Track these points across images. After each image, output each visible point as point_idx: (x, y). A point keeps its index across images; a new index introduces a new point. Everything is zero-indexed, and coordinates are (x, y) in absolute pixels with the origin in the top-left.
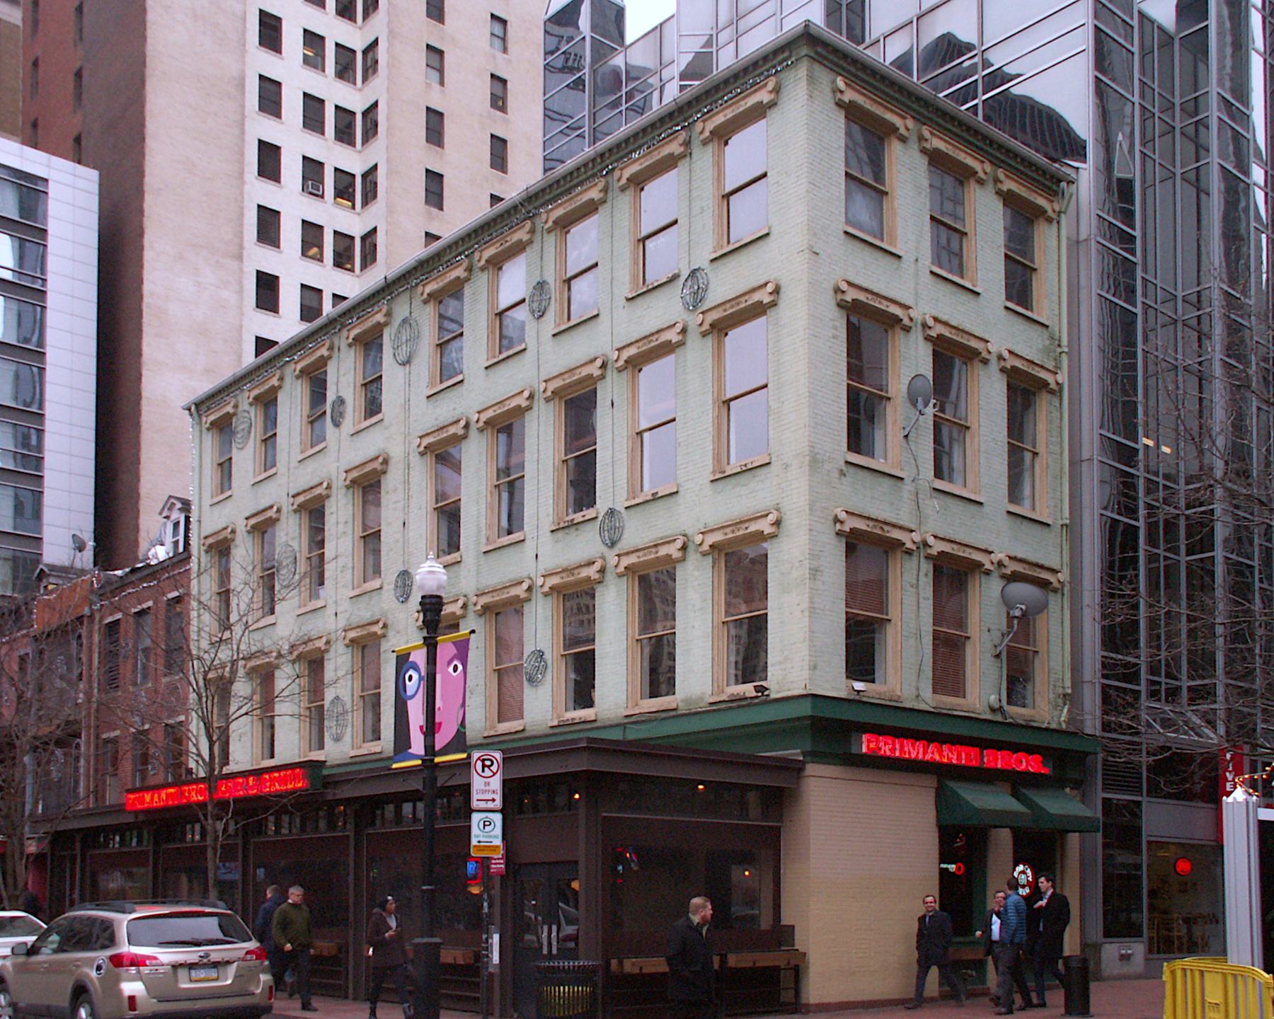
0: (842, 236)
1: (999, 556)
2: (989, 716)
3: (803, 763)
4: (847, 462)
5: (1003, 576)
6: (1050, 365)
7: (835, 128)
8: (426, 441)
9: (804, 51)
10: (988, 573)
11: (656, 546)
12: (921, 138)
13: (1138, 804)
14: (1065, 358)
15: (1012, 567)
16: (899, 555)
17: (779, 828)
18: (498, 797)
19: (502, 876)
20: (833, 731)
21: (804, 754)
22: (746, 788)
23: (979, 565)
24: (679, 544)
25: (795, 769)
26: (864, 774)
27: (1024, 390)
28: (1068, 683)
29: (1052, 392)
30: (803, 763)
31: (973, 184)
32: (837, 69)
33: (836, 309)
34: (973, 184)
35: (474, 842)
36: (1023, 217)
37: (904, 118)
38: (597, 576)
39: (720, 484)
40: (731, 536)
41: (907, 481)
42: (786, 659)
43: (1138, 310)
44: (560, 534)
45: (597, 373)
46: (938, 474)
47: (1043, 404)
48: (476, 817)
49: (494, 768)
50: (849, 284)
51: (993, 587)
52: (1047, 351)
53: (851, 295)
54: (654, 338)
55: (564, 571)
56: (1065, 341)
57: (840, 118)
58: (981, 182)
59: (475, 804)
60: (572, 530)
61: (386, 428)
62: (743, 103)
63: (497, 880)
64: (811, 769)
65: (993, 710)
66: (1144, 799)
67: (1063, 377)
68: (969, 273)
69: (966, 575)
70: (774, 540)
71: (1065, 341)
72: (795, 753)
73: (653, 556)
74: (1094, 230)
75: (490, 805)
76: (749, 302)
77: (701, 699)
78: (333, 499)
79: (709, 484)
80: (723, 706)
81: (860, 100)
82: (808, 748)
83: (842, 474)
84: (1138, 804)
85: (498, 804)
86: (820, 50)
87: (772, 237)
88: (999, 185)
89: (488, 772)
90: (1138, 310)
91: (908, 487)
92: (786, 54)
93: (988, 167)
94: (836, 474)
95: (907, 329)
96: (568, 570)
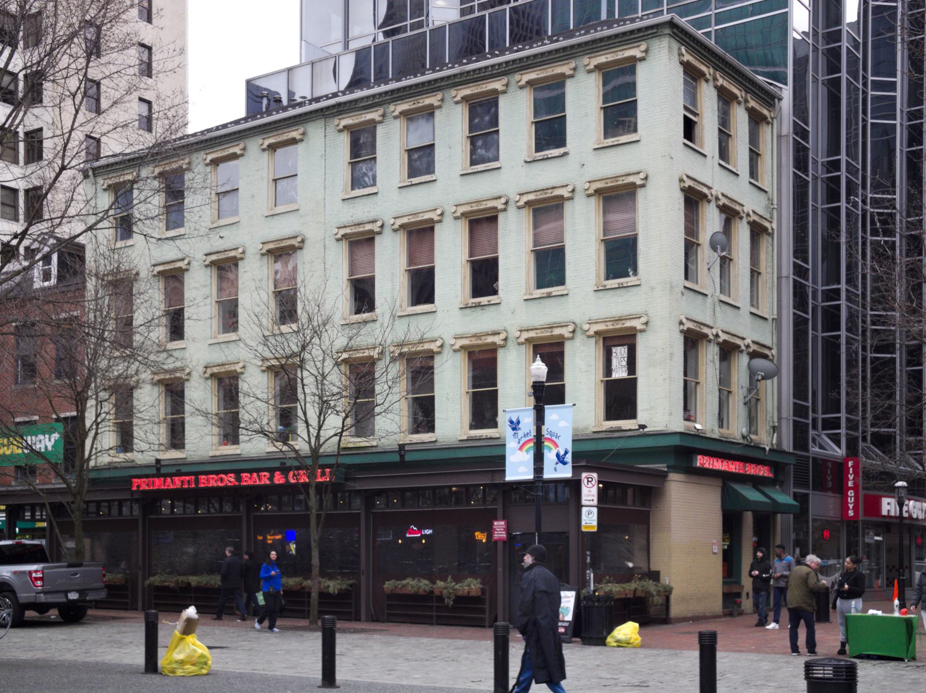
0: (682, 146)
1: (748, 341)
2: (741, 441)
3: (667, 472)
4: (685, 287)
5: (749, 354)
6: (768, 216)
7: (678, 76)
8: (342, 232)
9: (667, 31)
10: (710, 341)
11: (551, 328)
12: (681, 54)
13: (807, 495)
14: (775, 212)
15: (754, 347)
16: (705, 342)
17: (648, 512)
18: (596, 499)
19: (504, 542)
20: (683, 453)
21: (668, 467)
22: (625, 487)
23: (738, 347)
24: (571, 328)
25: (663, 476)
26: (694, 478)
27: (758, 231)
28: (776, 420)
29: (769, 234)
30: (667, 472)
31: (735, 104)
32: (682, 42)
33: (679, 191)
34: (735, 104)
35: (583, 523)
36: (756, 120)
37: (708, 67)
38: (502, 343)
39: (601, 294)
40: (611, 327)
41: (709, 296)
42: (652, 408)
43: (810, 179)
44: (468, 311)
45: (500, 207)
46: (686, 278)
47: (765, 242)
48: (584, 510)
49: (593, 482)
50: (688, 177)
51: (744, 359)
52: (767, 207)
53: (688, 183)
54: (549, 191)
55: (472, 336)
56: (775, 202)
57: (680, 70)
58: (707, 81)
59: (584, 502)
60: (478, 309)
61: (301, 216)
62: (621, 53)
63: (500, 545)
64: (673, 476)
65: (744, 437)
66: (810, 492)
67: (775, 226)
68: (732, 159)
69: (697, 341)
70: (644, 334)
71: (775, 202)
72: (662, 467)
73: (549, 334)
74: (791, 130)
75: (591, 503)
76: (625, 182)
77: (587, 429)
78: (246, 261)
79: (592, 292)
80: (600, 436)
81: (726, 84)
82: (672, 463)
83: (683, 294)
84: (807, 495)
85: (595, 502)
86: (675, 30)
87: (641, 143)
88: (682, 58)
89: (590, 485)
90: (810, 179)
91: (709, 300)
92: (654, 31)
93: (712, 71)
94: (680, 294)
95: (709, 201)
96: (476, 336)
